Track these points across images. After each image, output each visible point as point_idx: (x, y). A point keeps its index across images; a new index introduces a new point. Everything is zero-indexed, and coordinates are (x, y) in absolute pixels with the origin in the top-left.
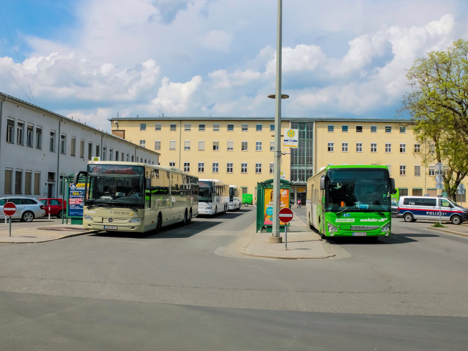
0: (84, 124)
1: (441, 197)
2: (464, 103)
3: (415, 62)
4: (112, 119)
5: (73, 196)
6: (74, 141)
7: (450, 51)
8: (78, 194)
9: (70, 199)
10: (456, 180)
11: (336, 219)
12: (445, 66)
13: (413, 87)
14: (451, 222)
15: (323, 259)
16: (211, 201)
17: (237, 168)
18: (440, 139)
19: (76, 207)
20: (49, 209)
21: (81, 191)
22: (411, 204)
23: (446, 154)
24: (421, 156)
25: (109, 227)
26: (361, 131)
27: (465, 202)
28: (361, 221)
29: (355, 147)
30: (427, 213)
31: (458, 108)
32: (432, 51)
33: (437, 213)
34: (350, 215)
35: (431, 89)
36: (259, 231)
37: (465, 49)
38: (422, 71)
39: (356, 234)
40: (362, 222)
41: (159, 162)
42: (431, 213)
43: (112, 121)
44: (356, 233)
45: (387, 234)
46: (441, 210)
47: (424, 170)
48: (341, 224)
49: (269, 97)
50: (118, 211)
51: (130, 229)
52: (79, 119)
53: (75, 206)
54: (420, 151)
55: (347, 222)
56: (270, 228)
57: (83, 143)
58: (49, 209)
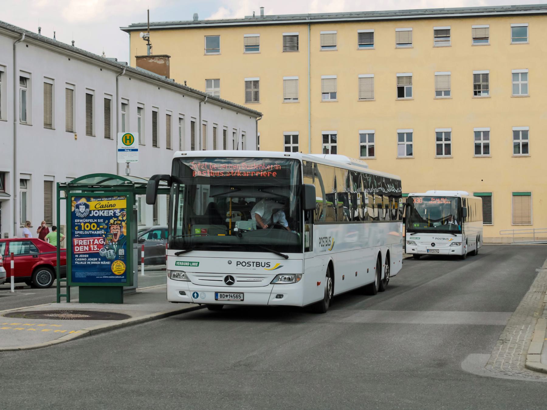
0: (71, 44)
4: (130, 26)
5: (81, 232)
6: (49, 88)
8: (94, 226)
9: (76, 241)
16: (297, 249)
20: (12, 266)
21: (102, 220)
25: (227, 296)
43: (134, 34)
50: (439, 237)
51: (273, 298)
52: (55, 33)
53: (87, 256)
57: (70, 92)
58: (12, 266)
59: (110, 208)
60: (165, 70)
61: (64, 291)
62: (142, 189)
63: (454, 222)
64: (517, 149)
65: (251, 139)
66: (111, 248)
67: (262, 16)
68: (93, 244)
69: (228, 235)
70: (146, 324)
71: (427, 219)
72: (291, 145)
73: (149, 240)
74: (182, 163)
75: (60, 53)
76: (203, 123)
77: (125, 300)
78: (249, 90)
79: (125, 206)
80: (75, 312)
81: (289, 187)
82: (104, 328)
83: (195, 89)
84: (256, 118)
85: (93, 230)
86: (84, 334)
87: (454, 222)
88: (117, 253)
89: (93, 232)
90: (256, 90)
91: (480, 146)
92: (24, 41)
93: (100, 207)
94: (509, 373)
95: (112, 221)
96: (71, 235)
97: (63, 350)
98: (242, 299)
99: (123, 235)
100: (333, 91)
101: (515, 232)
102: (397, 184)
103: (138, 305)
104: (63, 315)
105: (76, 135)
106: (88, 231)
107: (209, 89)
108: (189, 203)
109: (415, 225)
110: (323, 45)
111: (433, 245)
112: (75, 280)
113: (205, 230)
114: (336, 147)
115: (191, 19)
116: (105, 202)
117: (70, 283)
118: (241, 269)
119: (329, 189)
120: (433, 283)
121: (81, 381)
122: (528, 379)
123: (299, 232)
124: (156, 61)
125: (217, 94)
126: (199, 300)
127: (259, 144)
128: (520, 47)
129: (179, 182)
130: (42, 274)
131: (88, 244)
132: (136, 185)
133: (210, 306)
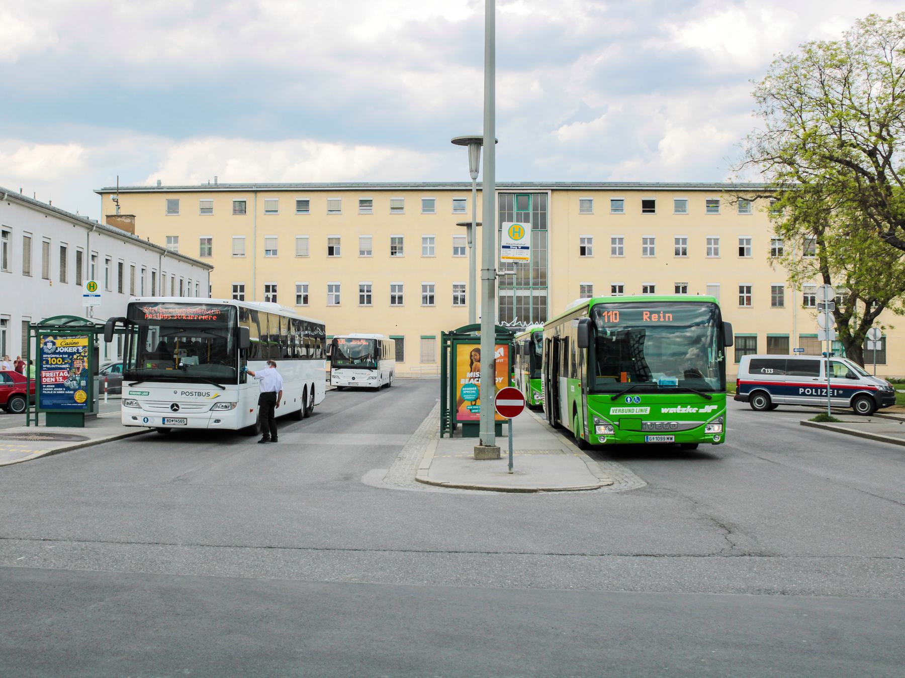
1: (829, 356)
2: (881, 154)
3: (773, 64)
5: (48, 366)
6: (27, 241)
7: (850, 39)
8: (59, 361)
9: (44, 374)
10: (864, 317)
11: (612, 409)
12: (839, 74)
13: (769, 120)
14: (851, 410)
15: (589, 491)
16: (233, 381)
17: (381, 296)
18: (827, 229)
19: (55, 389)
21: (67, 356)
22: (766, 372)
23: (842, 262)
24: (785, 267)
25: (173, 421)
26: (653, 211)
27: (885, 364)
28: (663, 412)
29: (705, 246)
30: (801, 390)
31: (867, 164)
32: (810, 42)
33: (822, 392)
34: (639, 400)
35: (808, 123)
36: (446, 435)
37: (884, 35)
38: (788, 84)
39: (653, 438)
40: (664, 413)
41: (210, 284)
42: (808, 391)
43: (105, 196)
44: (652, 437)
45: (718, 438)
46: (830, 384)
47: (793, 297)
48: (620, 418)
49: (306, 385)
51: (212, 423)
53: (54, 386)
54: (784, 253)
55: (635, 413)
56: (472, 428)
57: (46, 245)
59: (74, 345)
60: (131, 228)
61: (32, 416)
62: (102, 329)
63: (372, 360)
64: (425, 300)
65: (204, 289)
66: (74, 380)
67: (216, 184)
68: (59, 376)
69: (175, 369)
70: (102, 444)
71: (349, 357)
72: (239, 294)
73: (112, 373)
74: (136, 307)
75: (38, 211)
76: (162, 273)
77: (86, 424)
78: (203, 246)
79: (87, 344)
80: (42, 434)
81: (227, 329)
82: (65, 448)
83: (156, 244)
84: (209, 270)
85: (59, 365)
86: (47, 454)
87: (372, 360)
88: (79, 384)
89: (59, 366)
90: (209, 246)
91: (395, 297)
92: (6, 200)
93: (65, 344)
94: (402, 485)
95: (75, 357)
96: (40, 369)
97: (27, 467)
98: (185, 423)
99: (85, 369)
100: (274, 249)
101: (422, 368)
102: (322, 327)
103: (97, 429)
104: (30, 437)
105: (51, 282)
106: (55, 364)
107: (780, 246)
108: (142, 342)
109: (339, 362)
110: (267, 210)
111: (353, 378)
112: (42, 407)
113: (155, 364)
114: (339, 295)
115: (156, 185)
116: (69, 340)
117: (38, 410)
118: (184, 398)
119: (264, 332)
120: (353, 410)
121: (39, 494)
122: (416, 490)
123: (234, 367)
124: (123, 219)
125: (175, 249)
126: (149, 424)
127: (211, 292)
128: (429, 217)
129: (133, 324)
130: (16, 402)
131: (55, 376)
132: (97, 326)
133: (158, 429)
